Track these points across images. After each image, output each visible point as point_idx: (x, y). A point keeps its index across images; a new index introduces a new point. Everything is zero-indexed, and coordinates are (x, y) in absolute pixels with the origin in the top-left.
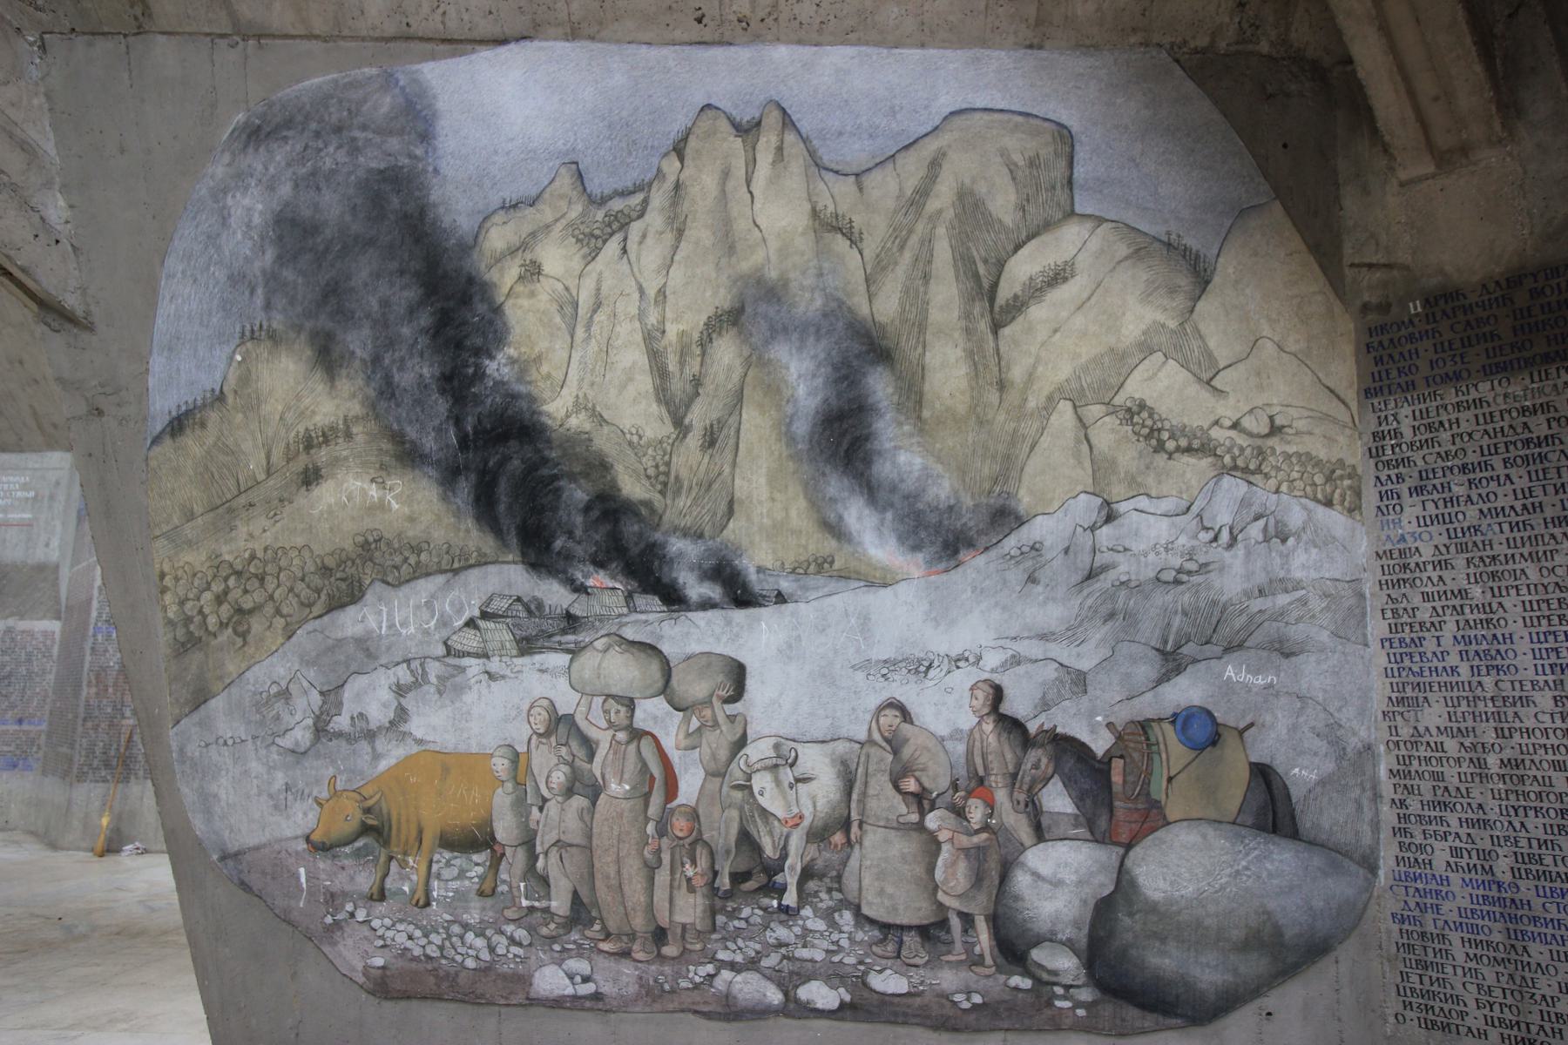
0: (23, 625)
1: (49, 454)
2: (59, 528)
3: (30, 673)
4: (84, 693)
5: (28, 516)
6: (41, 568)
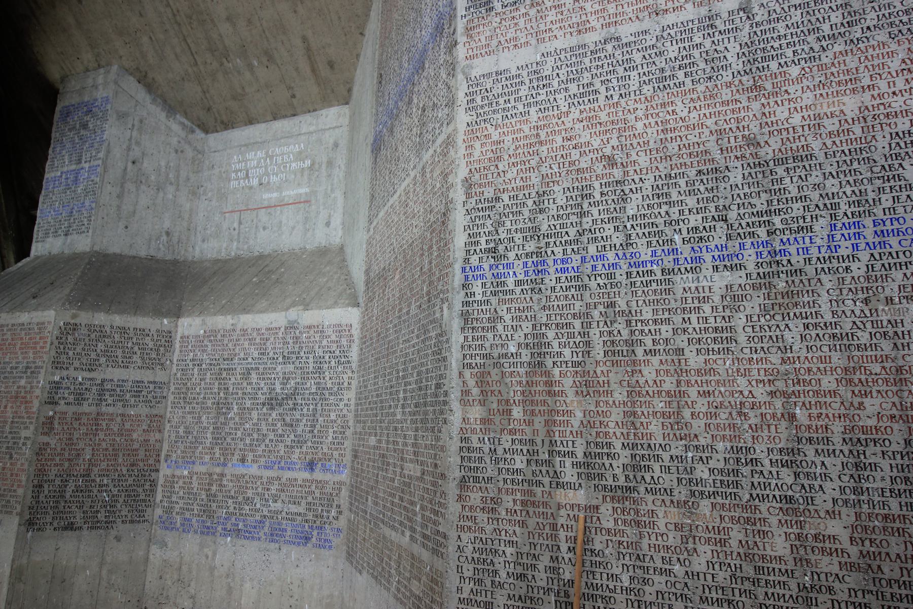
0: (309, 317)
1: (324, 112)
2: (340, 201)
3: (321, 388)
4: (456, 419)
5: (303, 190)
6: (323, 252)
